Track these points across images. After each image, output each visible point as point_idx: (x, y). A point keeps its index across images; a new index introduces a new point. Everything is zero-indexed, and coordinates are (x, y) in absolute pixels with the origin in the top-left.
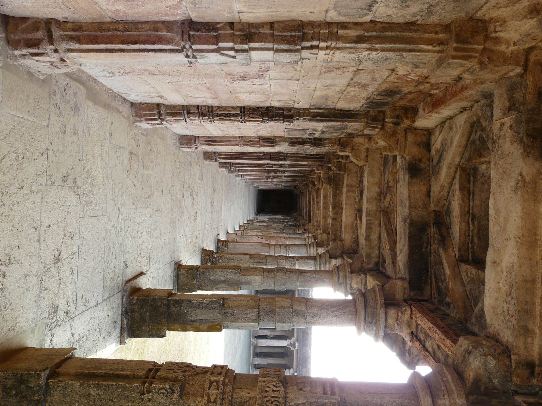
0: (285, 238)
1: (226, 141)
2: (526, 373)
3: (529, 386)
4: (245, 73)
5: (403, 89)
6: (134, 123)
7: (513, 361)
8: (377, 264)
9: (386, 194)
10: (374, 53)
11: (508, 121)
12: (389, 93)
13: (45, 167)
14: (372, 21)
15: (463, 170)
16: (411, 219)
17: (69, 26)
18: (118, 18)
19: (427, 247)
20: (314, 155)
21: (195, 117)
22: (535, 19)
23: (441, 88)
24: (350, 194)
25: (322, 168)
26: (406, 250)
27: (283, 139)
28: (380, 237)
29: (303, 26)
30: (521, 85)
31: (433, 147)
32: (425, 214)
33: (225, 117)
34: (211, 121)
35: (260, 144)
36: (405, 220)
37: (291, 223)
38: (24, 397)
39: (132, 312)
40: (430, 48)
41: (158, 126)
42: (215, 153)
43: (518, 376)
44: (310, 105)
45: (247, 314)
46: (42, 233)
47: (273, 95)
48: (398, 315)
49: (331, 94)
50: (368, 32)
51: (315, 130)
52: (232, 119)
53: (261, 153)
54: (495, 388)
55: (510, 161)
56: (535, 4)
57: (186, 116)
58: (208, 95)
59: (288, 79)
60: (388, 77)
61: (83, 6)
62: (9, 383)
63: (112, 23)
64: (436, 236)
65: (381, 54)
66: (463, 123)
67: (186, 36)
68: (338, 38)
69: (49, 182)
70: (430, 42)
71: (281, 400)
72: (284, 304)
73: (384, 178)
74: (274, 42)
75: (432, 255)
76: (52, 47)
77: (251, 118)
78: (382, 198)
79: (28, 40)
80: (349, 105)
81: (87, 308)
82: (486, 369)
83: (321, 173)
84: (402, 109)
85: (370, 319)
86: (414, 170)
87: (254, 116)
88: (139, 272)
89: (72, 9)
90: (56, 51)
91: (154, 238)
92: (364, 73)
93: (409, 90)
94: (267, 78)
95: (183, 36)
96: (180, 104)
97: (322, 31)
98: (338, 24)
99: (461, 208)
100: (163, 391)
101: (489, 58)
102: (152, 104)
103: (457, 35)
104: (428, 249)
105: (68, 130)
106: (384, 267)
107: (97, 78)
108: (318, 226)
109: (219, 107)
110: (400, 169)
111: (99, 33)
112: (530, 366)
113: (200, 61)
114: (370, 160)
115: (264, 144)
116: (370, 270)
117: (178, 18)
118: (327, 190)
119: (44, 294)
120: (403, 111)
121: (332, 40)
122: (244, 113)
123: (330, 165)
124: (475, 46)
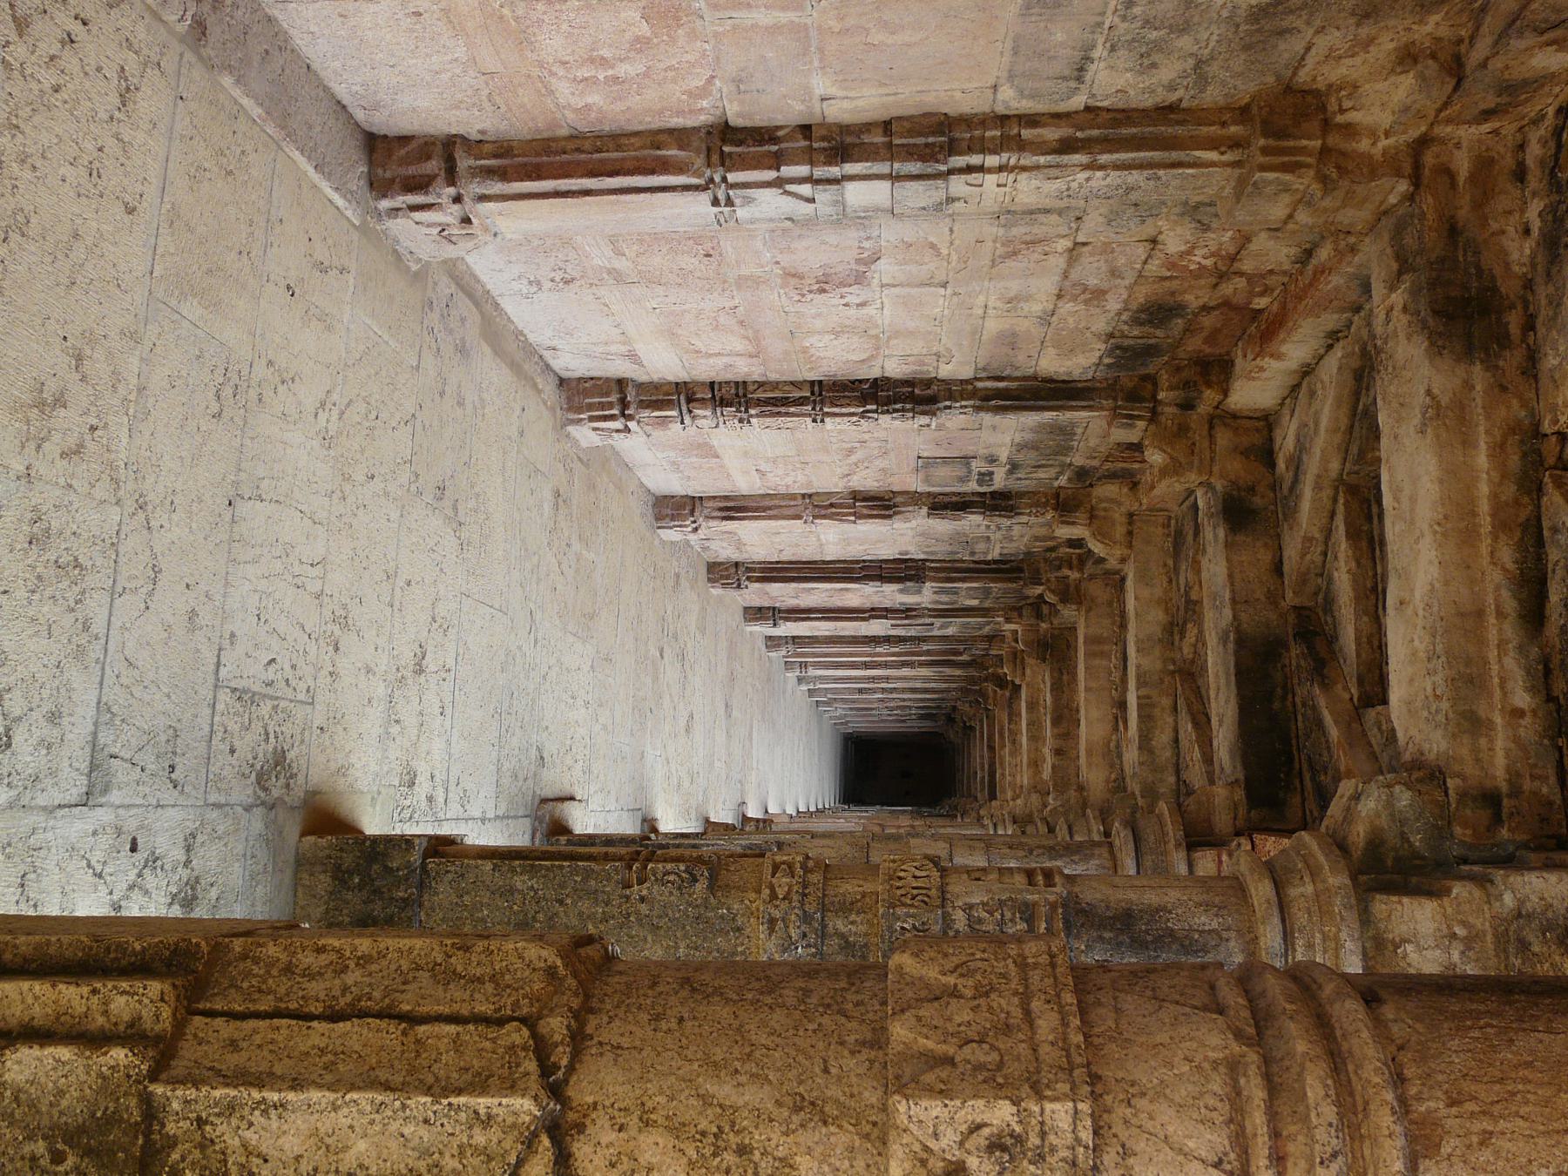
1: (770, 508)
2: (1484, 816)
3: (1494, 845)
5: (1187, 297)
6: (564, 426)
7: (1450, 791)
9: (1185, 623)
10: (1099, 174)
11: (1398, 298)
12: (1157, 312)
14: (1088, 109)
15: (1353, 490)
16: (1238, 631)
17: (487, 148)
18: (583, 127)
19: (1284, 698)
20: (995, 562)
22: (1411, 74)
23: (1273, 290)
24: (1097, 662)
25: (1020, 616)
27: (915, 498)
28: (1176, 741)
29: (950, 125)
31: (1281, 455)
32: (1273, 616)
34: (741, 421)
35: (854, 514)
36: (1224, 640)
40: (1212, 156)
42: (737, 564)
43: (1465, 825)
46: (398, 591)
47: (889, 338)
48: (1220, 862)
49: (1023, 325)
50: (1082, 129)
51: (992, 460)
53: (858, 562)
54: (1416, 855)
56: (1406, 46)
57: (684, 408)
58: (739, 345)
59: (922, 285)
60: (1145, 262)
61: (526, 100)
62: (348, 860)
63: (571, 137)
64: (1302, 663)
65: (1114, 177)
67: (715, 158)
68: (1022, 146)
69: (413, 488)
70: (1212, 144)
71: (933, 892)
74: (892, 159)
75: (1300, 718)
76: (451, 191)
78: (1177, 638)
79: (407, 178)
81: (466, 815)
82: (1392, 815)
84: (1196, 363)
86: (1239, 513)
87: (843, 401)
90: (457, 199)
92: (1091, 255)
93: (1201, 302)
94: (876, 281)
95: (708, 156)
96: (671, 378)
97: (988, 134)
98: (1019, 117)
99: (1354, 581)
100: (671, 878)
101: (1338, 165)
102: (607, 380)
103: (1264, 122)
104: (1289, 704)
109: (761, 385)
112: (1491, 799)
113: (741, 213)
115: (865, 511)
117: (702, 119)
118: (1037, 679)
119: (395, 729)
120: (1198, 369)
121: (1009, 150)
124: (1305, 142)
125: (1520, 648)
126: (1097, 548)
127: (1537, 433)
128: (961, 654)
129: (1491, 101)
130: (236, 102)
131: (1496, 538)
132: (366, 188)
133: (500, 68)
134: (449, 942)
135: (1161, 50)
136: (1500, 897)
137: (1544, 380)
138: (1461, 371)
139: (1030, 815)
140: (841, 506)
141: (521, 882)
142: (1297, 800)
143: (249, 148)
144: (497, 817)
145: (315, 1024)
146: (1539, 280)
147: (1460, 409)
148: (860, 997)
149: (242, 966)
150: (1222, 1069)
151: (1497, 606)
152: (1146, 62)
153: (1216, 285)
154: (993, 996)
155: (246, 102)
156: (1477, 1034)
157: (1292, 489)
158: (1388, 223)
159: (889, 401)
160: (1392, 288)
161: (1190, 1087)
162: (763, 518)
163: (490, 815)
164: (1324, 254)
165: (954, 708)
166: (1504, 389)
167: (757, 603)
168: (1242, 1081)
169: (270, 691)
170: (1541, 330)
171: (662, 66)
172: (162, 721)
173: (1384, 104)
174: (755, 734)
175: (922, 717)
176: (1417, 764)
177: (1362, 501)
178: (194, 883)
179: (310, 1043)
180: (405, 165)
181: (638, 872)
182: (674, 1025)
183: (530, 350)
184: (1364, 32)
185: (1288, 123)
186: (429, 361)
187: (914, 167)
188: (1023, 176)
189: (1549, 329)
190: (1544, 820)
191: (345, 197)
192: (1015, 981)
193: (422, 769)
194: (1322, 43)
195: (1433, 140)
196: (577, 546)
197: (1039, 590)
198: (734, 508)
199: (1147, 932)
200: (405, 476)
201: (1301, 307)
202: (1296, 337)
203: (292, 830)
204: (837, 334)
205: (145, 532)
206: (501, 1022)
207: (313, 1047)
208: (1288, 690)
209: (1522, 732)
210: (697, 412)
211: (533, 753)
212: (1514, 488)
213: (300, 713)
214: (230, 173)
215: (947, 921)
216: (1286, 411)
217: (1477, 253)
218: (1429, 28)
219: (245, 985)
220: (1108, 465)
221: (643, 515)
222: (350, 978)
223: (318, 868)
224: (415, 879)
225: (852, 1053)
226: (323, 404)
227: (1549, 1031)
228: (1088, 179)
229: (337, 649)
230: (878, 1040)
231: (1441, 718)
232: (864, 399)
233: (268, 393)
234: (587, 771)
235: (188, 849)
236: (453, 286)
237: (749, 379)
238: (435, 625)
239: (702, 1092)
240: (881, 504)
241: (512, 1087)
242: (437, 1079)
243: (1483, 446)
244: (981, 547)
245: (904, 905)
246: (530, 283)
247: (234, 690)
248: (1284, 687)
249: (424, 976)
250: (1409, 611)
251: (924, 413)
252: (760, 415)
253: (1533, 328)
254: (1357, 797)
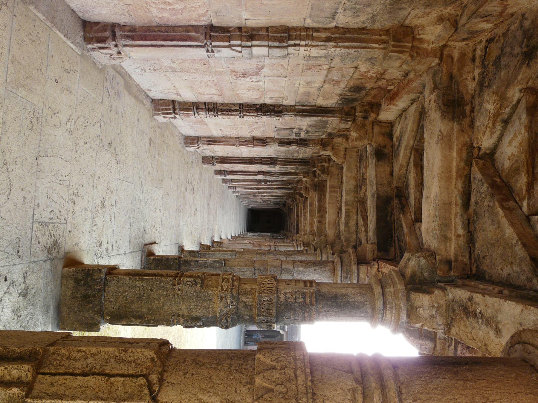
1: (224, 141)
2: (446, 267)
4: (246, 71)
6: (153, 116)
7: (437, 260)
9: (362, 186)
10: (339, 49)
11: (433, 97)
12: (357, 89)
13: (99, 132)
14: (336, 27)
15: (417, 151)
16: (378, 194)
17: (127, 28)
18: (161, 23)
19: (391, 216)
20: (300, 159)
22: (441, 25)
24: (333, 194)
25: (308, 176)
27: (274, 140)
28: (357, 224)
29: (289, 30)
30: (439, 71)
32: (389, 189)
34: (215, 116)
35: (253, 144)
36: (373, 196)
38: (90, 287)
40: (377, 45)
42: (213, 157)
43: (440, 270)
44: (296, 102)
45: (244, 272)
46: (95, 181)
48: (368, 270)
49: (312, 90)
51: (300, 129)
53: (254, 158)
55: (434, 123)
57: (195, 111)
58: (215, 92)
59: (278, 76)
60: (353, 74)
62: (80, 276)
63: (157, 26)
65: (344, 50)
66: (413, 112)
67: (208, 36)
68: (313, 38)
69: (101, 145)
70: (377, 42)
71: (274, 289)
74: (269, 41)
76: (114, 43)
78: (359, 190)
82: (419, 267)
85: (345, 275)
86: (381, 155)
87: (250, 111)
89: (133, 16)
90: (116, 46)
93: (371, 86)
94: (262, 75)
95: (205, 36)
96: (191, 101)
98: (313, 29)
100: (189, 283)
101: (417, 52)
102: (169, 100)
103: (393, 36)
104: (392, 218)
105: (113, 109)
107: (131, 75)
109: (222, 104)
111: (148, 33)
112: (449, 262)
113: (216, 55)
114: (347, 158)
115: (257, 144)
117: (204, 23)
118: (313, 196)
119: (95, 228)
121: (309, 39)
124: (407, 44)
125: (461, 215)
126: (334, 158)
127: (472, 147)
128: (288, 185)
129: (466, 36)
130: (35, 15)
131: (457, 180)
132: (83, 41)
133: (132, 3)
134: (120, 349)
135: (361, 11)
136: (448, 295)
137: (475, 130)
138: (450, 124)
139: (309, 242)
140: (249, 141)
141: (138, 284)
142: (393, 249)
143: (40, 31)
144: (130, 252)
145: (78, 377)
146: (477, 96)
147: (449, 136)
148: (246, 367)
149: (53, 357)
150: (351, 392)
151: (456, 202)
152: (356, 15)
153: (376, 82)
154: (286, 369)
155: (39, 15)
156: (423, 379)
157: (398, 148)
158: (432, 71)
160: (431, 93)
161: (341, 397)
162: (222, 145)
163: (127, 252)
164: (411, 75)
165: (286, 201)
166: (463, 131)
167: (219, 169)
168: (356, 395)
169: (52, 221)
170: (476, 113)
171: (190, 6)
172: (15, 236)
173: (432, 33)
174: (217, 212)
175: (274, 204)
176: (428, 250)
177: (418, 152)
178: (26, 289)
179: (77, 384)
180: (97, 33)
181: (178, 281)
182: (190, 376)
183: (141, 91)
184: (427, 10)
185: (401, 37)
186: (106, 99)
187: (276, 44)
188: (313, 49)
189: (478, 113)
190: (464, 269)
191: (75, 45)
192: (293, 364)
193: (104, 240)
194: (413, 13)
195: (447, 45)
196: (157, 157)
197: (315, 169)
198: (212, 141)
199: (341, 302)
200: (98, 141)
201: (403, 92)
202: (402, 100)
203: (60, 267)
204: (248, 90)
205: (7, 173)
206: (137, 376)
207: (78, 385)
208: (392, 214)
209: (460, 242)
210: (200, 113)
211: (142, 229)
212: (463, 164)
213: (62, 227)
214: (33, 41)
215: (278, 298)
216: (397, 122)
217: (458, 85)
218: (448, 11)
219: (55, 363)
220: (339, 133)
221: (180, 143)
222: (89, 361)
223: (69, 279)
224: (102, 283)
225: (244, 386)
226: (69, 120)
227: (443, 378)
228: (335, 51)
229: (74, 204)
230: (251, 382)
231: (436, 236)
232: (257, 110)
233: (49, 119)
234: (160, 233)
235: (24, 278)
236: (114, 72)
238: (108, 191)
239: (199, 398)
240: (262, 141)
241: (141, 399)
242: (118, 396)
243: (455, 150)
244: (296, 154)
245: (265, 293)
246: (142, 70)
247: (39, 222)
248: (391, 213)
249: (113, 360)
250: (429, 200)
251: (278, 116)
252: (222, 115)
253: (473, 112)
254: (409, 260)
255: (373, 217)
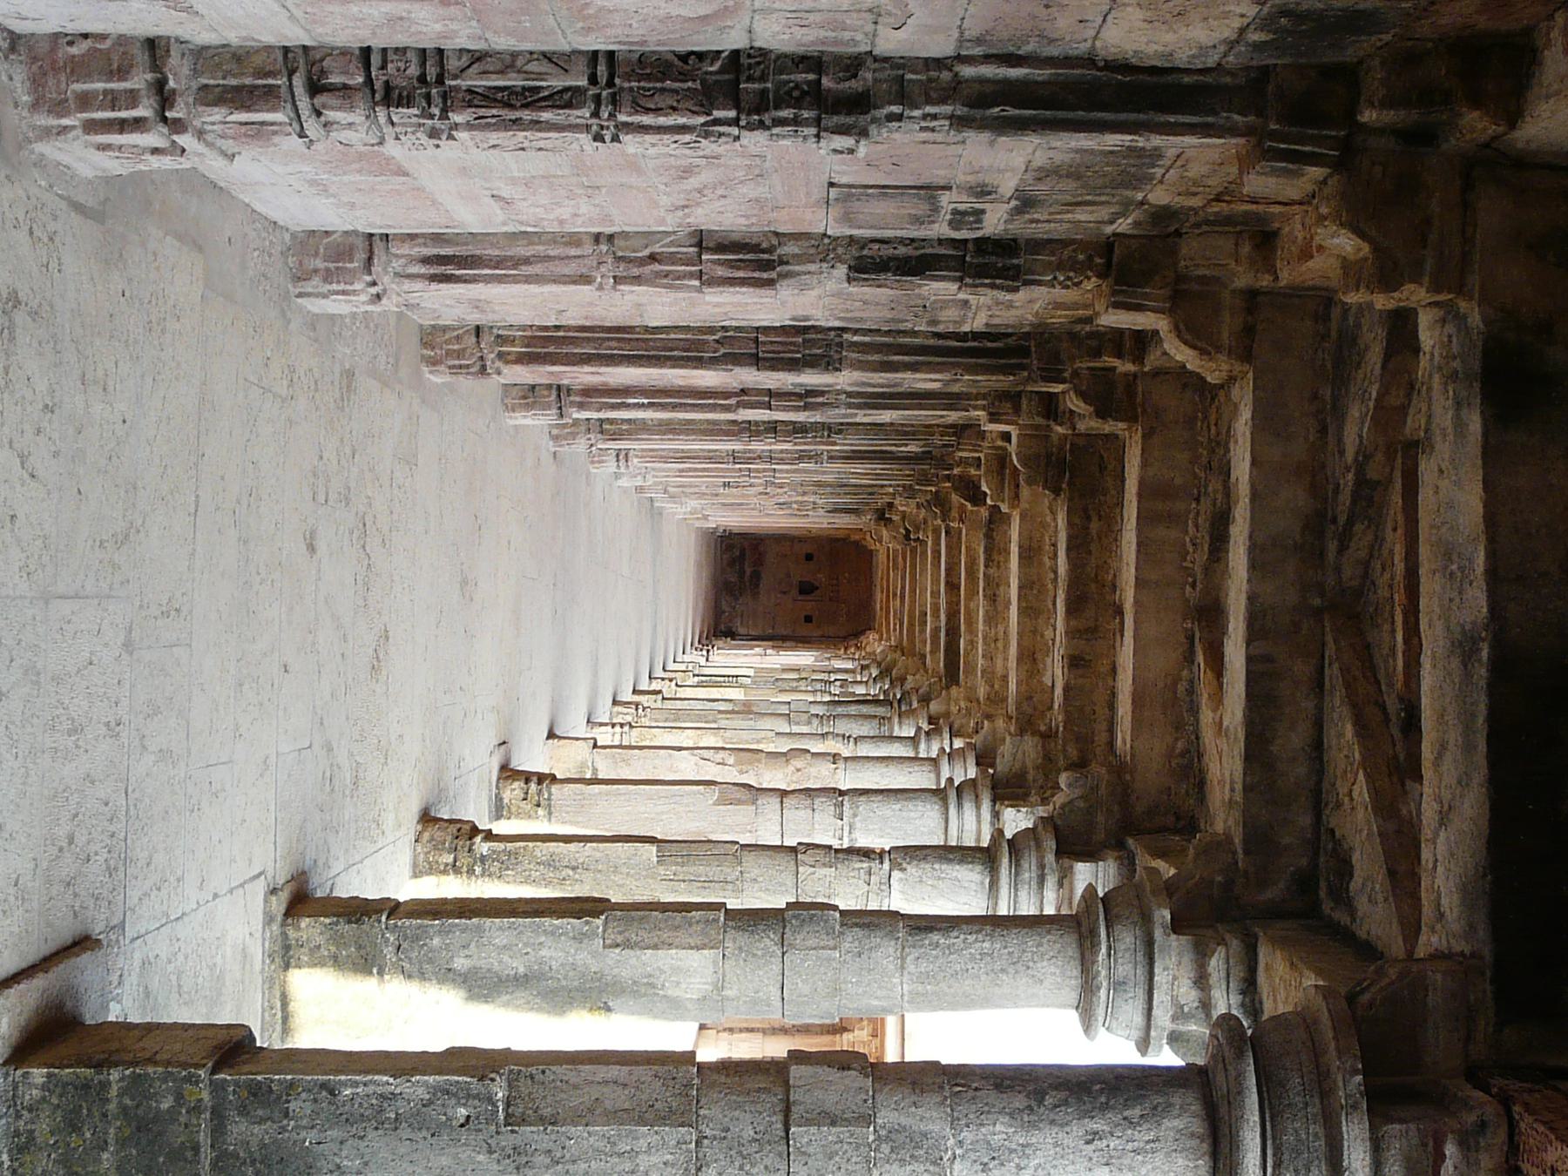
0: (835, 757)
1: (527, 261)
8: (1305, 883)
9: (1350, 522)
16: (1497, 644)
20: (976, 336)
21: (352, 108)
24: (1161, 532)
25: (1017, 410)
26: (1472, 806)
27: (823, 249)
33: (509, 105)
34: (434, 134)
36: (1464, 647)
37: (860, 690)
39: (21, 1149)
41: (155, 162)
42: (478, 330)
44: (961, 41)
51: (983, 191)
52: (546, 116)
53: (711, 330)
57: (304, 103)
72: (830, 1100)
73: (1340, 441)
77: (648, 110)
78: (1332, 546)
80: (1169, 37)
83: (1006, 437)
88: (65, 936)
91: (149, 759)
96: (268, 39)
102: (123, 40)
106: (1342, 897)
108: (997, 699)
109: (478, 57)
110: (1436, 378)
115: (720, 272)
116: (1274, 914)
122: (610, 84)
123: (1057, 388)
140: (672, 259)
159: (761, 104)
162: (515, 280)
165: (890, 505)
210: (331, 115)
220: (1216, 208)
232: (706, 99)
237: (447, 45)
255: (1463, 782)
